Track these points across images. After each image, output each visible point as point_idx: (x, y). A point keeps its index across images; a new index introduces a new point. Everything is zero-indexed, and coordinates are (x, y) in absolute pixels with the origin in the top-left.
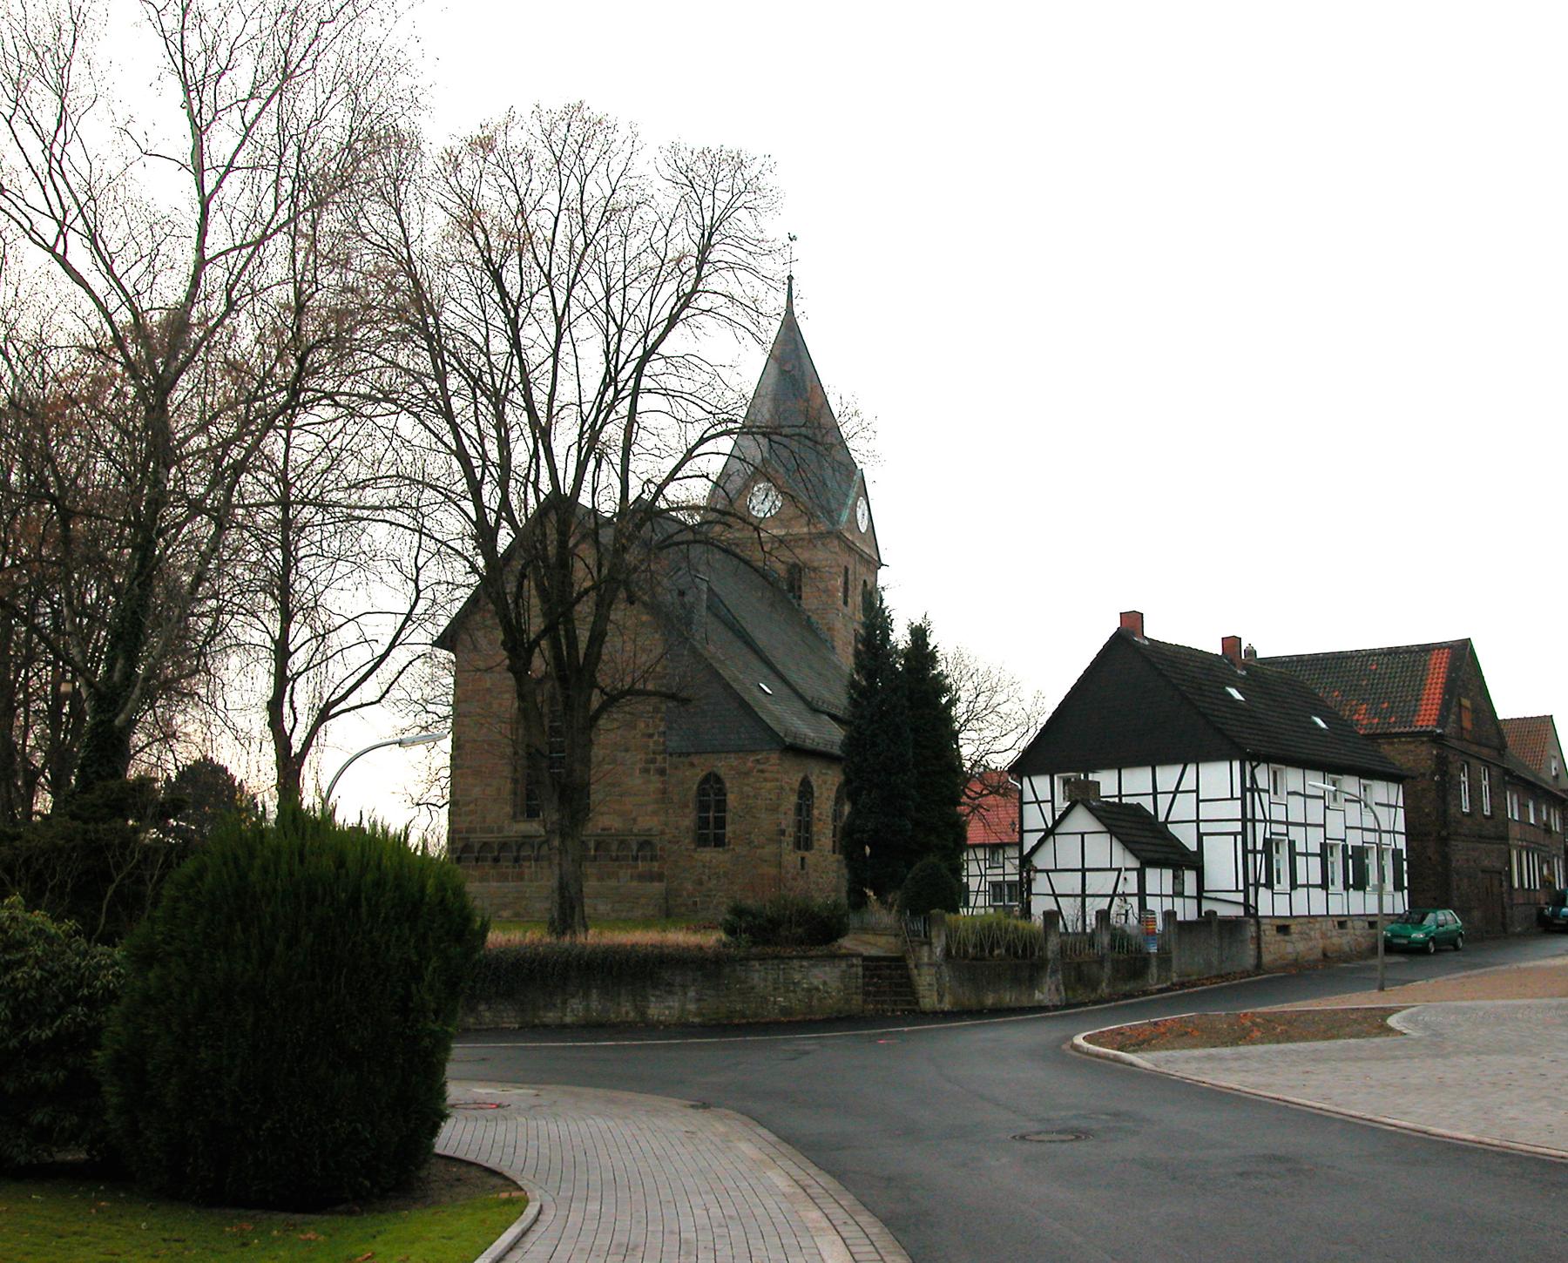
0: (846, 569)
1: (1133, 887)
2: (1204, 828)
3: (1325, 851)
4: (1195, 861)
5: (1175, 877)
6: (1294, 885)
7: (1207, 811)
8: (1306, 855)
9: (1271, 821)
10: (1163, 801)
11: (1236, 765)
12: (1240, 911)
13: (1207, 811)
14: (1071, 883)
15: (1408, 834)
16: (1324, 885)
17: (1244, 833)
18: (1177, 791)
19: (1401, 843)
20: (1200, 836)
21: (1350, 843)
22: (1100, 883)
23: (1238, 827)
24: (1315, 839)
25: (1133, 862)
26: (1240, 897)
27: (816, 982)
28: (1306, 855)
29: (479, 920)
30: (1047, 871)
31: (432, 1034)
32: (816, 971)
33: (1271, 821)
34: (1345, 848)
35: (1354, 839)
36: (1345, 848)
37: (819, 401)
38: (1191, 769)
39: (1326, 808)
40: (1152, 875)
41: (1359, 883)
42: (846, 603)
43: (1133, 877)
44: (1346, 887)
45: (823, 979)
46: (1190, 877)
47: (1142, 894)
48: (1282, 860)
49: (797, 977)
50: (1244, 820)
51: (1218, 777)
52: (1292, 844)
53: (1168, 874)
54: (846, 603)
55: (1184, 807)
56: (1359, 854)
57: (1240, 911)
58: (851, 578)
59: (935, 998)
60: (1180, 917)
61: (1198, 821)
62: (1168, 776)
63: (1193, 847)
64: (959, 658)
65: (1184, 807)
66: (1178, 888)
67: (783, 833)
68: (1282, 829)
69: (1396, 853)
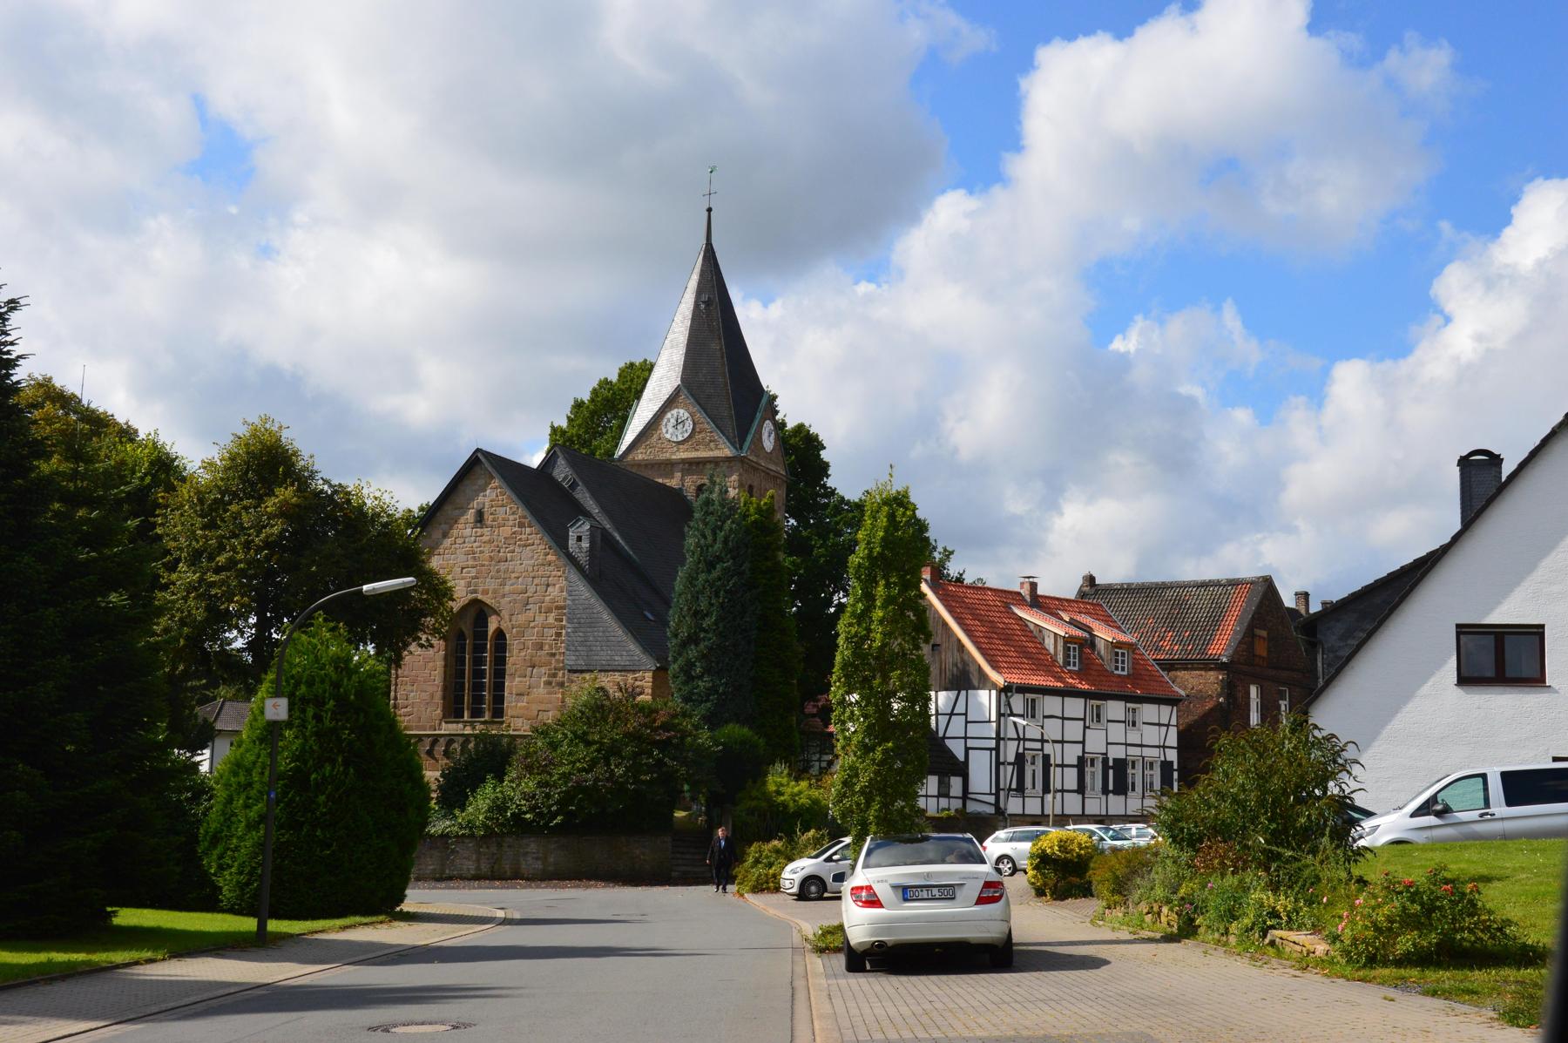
2: (970, 743)
3: (1081, 764)
4: (962, 770)
5: (940, 783)
6: (1046, 789)
7: (973, 730)
8: (1063, 766)
9: (1025, 740)
12: (991, 810)
13: (973, 730)
15: (1182, 748)
16: (1081, 789)
17: (997, 749)
19: (1172, 756)
20: (967, 749)
21: (1111, 756)
23: (993, 744)
24: (1072, 754)
26: (992, 799)
28: (1063, 766)
31: (477, 745)
33: (1025, 740)
34: (1105, 761)
35: (1116, 753)
36: (1105, 761)
37: (530, 864)
38: (963, 693)
39: (1085, 727)
41: (1122, 788)
44: (1105, 791)
46: (956, 783)
48: (1033, 770)
52: (1046, 758)
55: (957, 726)
56: (1121, 766)
57: (991, 810)
61: (966, 738)
63: (961, 758)
64: (871, 486)
65: (957, 726)
66: (944, 791)
68: (1038, 745)
69: (1166, 766)
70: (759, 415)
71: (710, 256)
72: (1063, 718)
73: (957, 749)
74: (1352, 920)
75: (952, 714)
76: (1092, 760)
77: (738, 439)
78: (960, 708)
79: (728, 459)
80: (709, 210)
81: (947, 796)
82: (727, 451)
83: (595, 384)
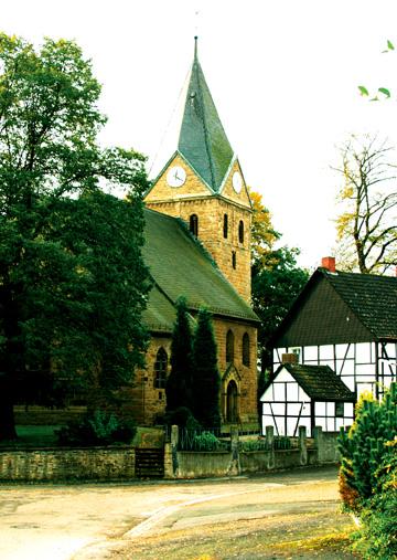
0: (226, 216)
1: (307, 411)
2: (358, 379)
5: (336, 407)
7: (360, 370)
10: (339, 363)
11: (373, 344)
13: (360, 370)
14: (279, 409)
18: (345, 359)
20: (356, 383)
22: (293, 410)
25: (309, 399)
27: (112, 461)
29: (69, 144)
30: (270, 403)
32: (111, 456)
38: (352, 345)
40: (320, 407)
42: (225, 236)
43: (308, 406)
45: (116, 459)
47: (313, 416)
49: (102, 458)
50: (377, 375)
51: (365, 350)
53: (331, 405)
54: (225, 236)
58: (229, 220)
59: (96, 369)
60: (324, 430)
62: (341, 348)
63: (352, 390)
65: (348, 368)
66: (339, 413)
67: (146, 379)
70: (230, 169)
71: (197, 72)
72: (286, 403)
73: (349, 383)
74: (148, 422)
75: (345, 359)
76: (67, 465)
77: (214, 185)
78: (351, 355)
79: (209, 198)
80: (196, 38)
81: (342, 416)
82: (208, 193)
83: (98, 74)
